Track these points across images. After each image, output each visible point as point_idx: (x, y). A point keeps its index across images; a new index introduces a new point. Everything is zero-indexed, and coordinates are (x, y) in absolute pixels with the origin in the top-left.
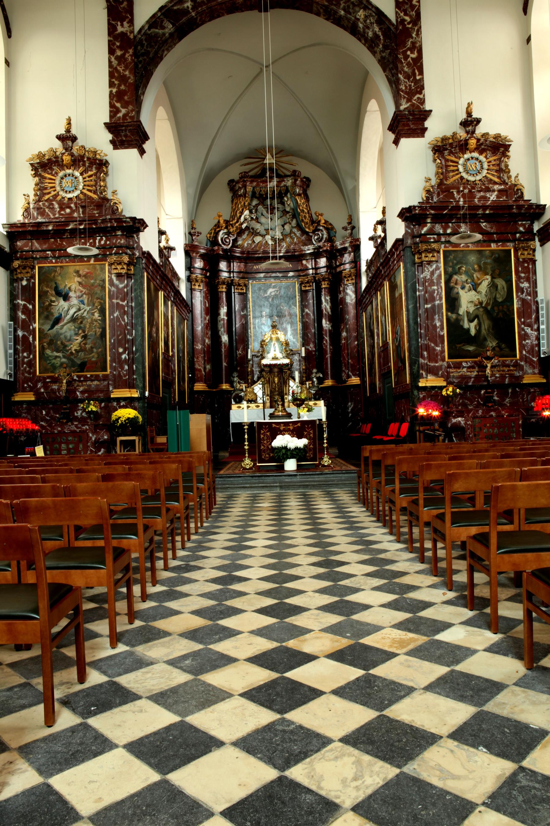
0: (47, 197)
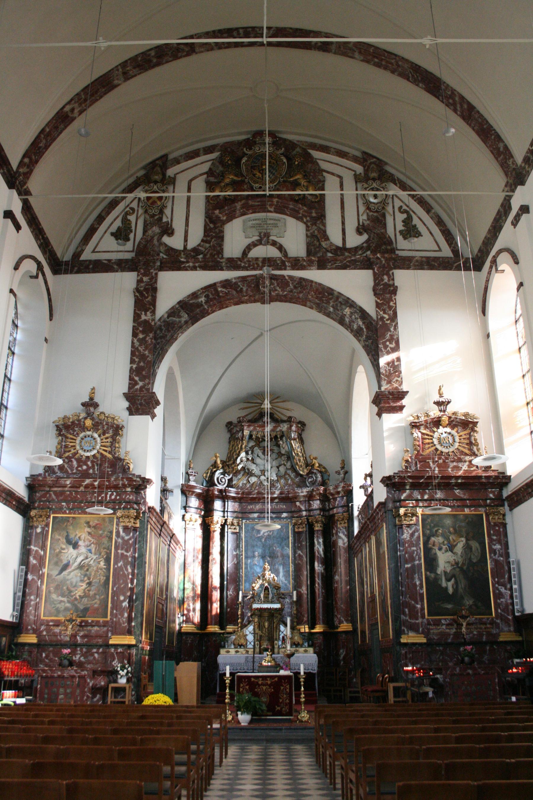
0: (67, 454)
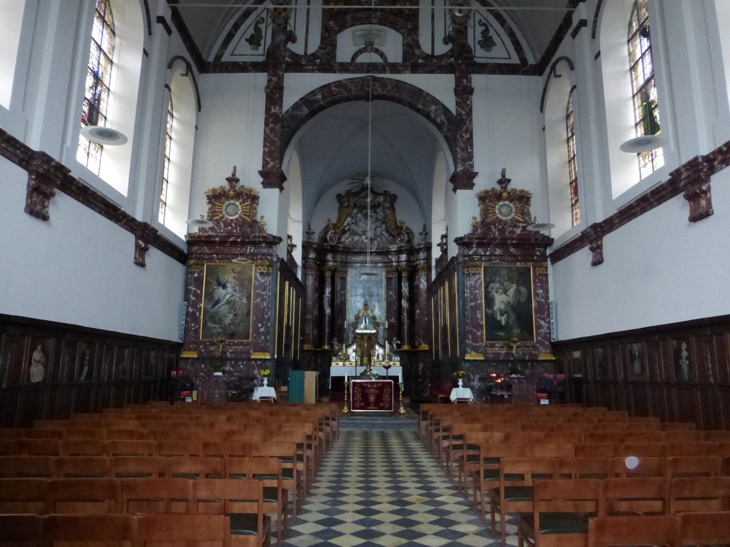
0: (216, 218)
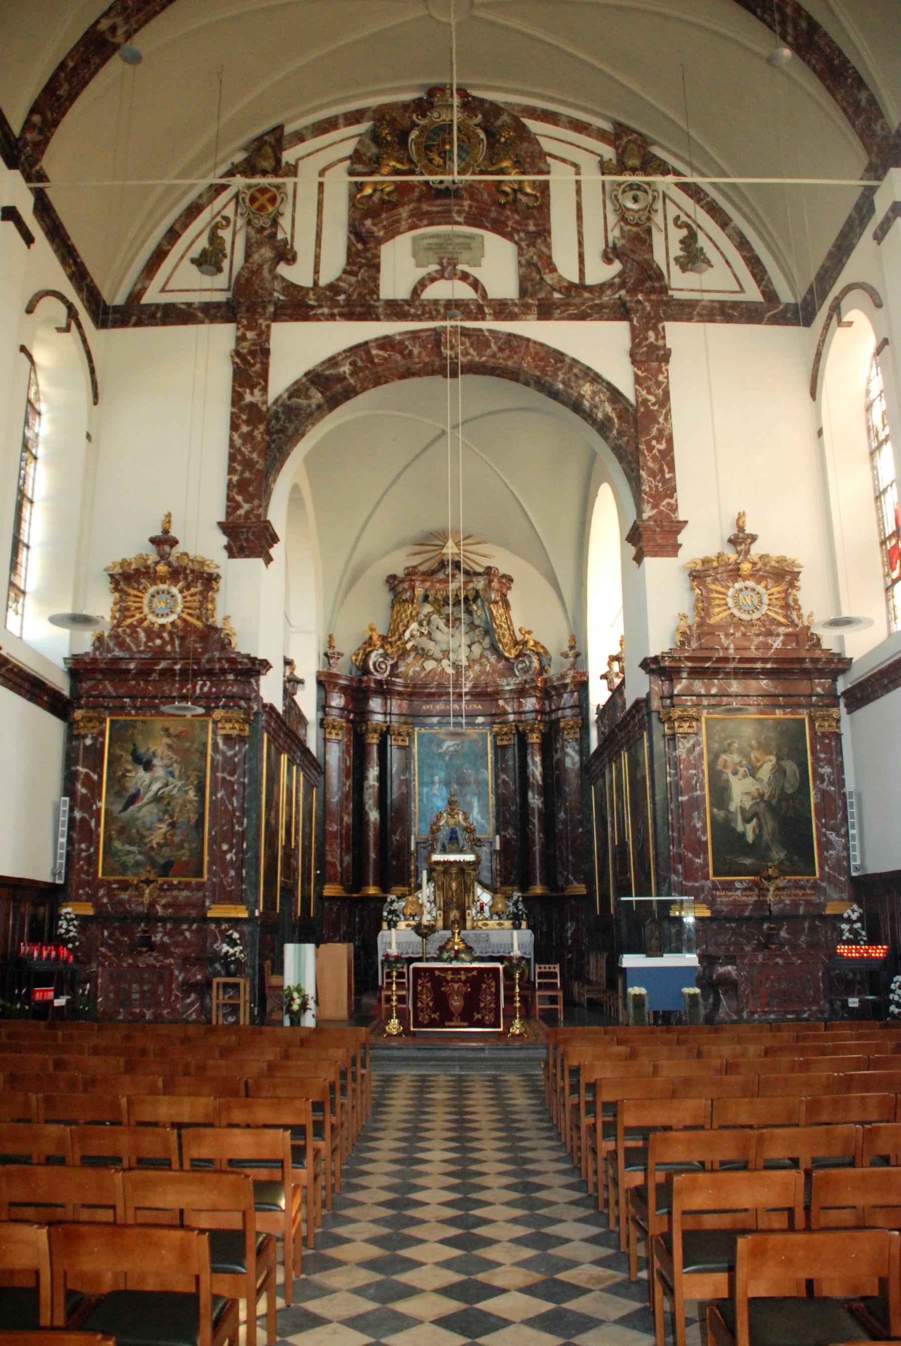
0: (129, 621)
